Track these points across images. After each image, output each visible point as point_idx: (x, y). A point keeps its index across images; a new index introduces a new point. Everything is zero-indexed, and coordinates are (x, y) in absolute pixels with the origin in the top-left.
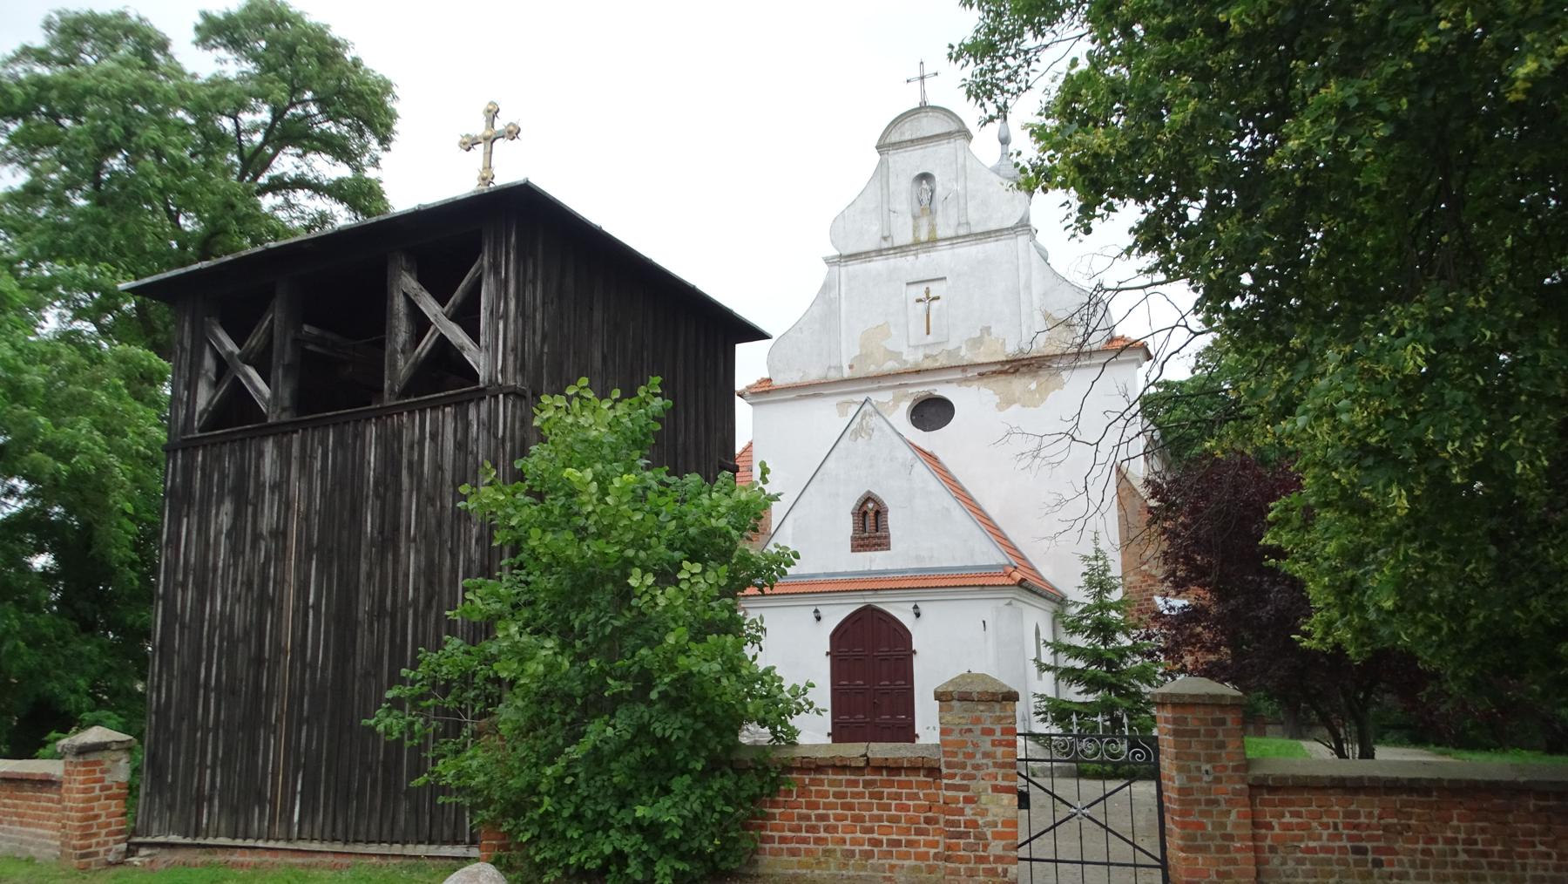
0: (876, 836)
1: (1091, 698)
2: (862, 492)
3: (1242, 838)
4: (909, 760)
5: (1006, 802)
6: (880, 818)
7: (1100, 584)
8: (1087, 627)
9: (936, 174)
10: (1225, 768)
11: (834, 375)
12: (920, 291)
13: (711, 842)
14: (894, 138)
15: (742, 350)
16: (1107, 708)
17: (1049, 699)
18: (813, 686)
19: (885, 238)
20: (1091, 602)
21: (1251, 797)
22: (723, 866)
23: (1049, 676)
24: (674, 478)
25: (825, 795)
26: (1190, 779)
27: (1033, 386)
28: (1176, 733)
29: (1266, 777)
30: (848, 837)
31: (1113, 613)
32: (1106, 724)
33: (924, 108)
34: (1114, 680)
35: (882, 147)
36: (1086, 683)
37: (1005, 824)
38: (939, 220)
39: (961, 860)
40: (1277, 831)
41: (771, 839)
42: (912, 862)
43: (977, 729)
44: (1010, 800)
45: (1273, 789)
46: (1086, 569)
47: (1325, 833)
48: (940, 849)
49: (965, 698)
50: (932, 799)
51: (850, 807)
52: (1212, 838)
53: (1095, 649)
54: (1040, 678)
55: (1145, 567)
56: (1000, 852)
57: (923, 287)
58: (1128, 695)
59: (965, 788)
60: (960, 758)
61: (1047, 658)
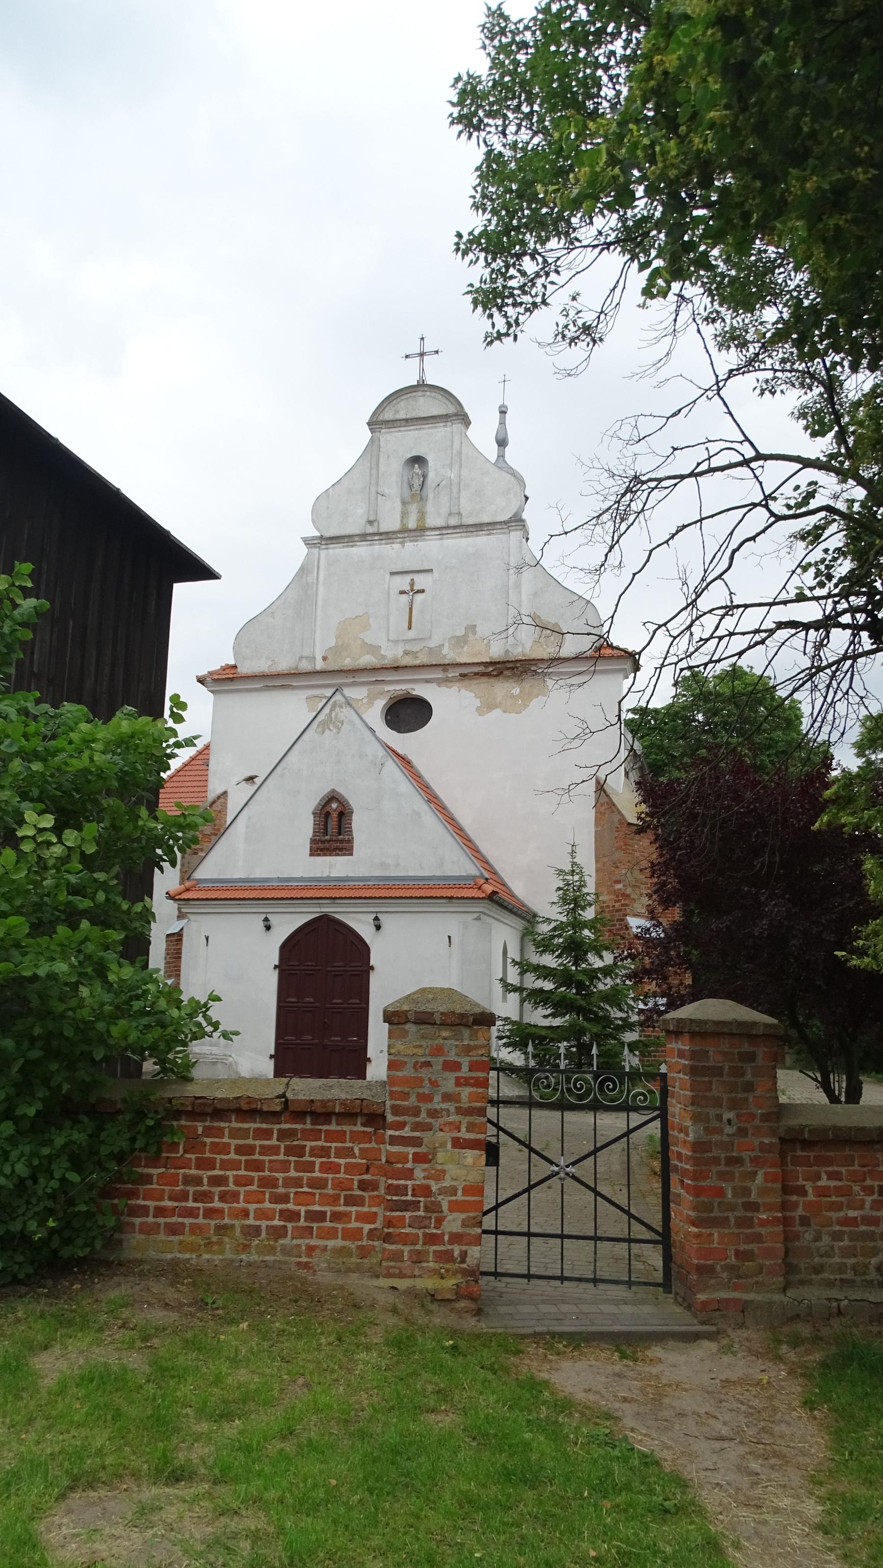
0: (291, 1206)
1: (557, 1022)
2: (325, 791)
3: (769, 1208)
4: (343, 1103)
5: (469, 1161)
6: (298, 1182)
7: (575, 900)
8: (559, 946)
9: (430, 459)
10: (753, 1116)
11: (305, 666)
12: (403, 582)
13: (42, 1223)
14: (388, 415)
15: (182, 592)
16: (572, 1033)
17: (514, 1023)
18: (219, 999)
19: (371, 522)
20: (564, 919)
21: (782, 1154)
22: (66, 1253)
23: (514, 997)
24: (45, 707)
25: (224, 1149)
26: (708, 1131)
27: (516, 691)
28: (693, 1071)
29: (802, 1128)
30: (252, 1207)
31: (586, 932)
32: (575, 1047)
33: (421, 386)
34: (583, 1003)
35: (374, 424)
36: (554, 1006)
37: (467, 1191)
38: (430, 508)
39: (405, 1239)
40: (811, 1197)
41: (143, 1211)
42: (339, 1243)
43: (438, 1062)
44: (473, 1157)
45: (807, 1144)
46: (561, 884)
47: (869, 1200)
48: (378, 1225)
49: (424, 1019)
50: (371, 1156)
51: (257, 1166)
52: (732, 1208)
53: (566, 970)
54: (505, 999)
55: (619, 886)
56: (457, 1228)
57: (407, 578)
58: (597, 1019)
59: (416, 1142)
60: (413, 1101)
61: (513, 977)
